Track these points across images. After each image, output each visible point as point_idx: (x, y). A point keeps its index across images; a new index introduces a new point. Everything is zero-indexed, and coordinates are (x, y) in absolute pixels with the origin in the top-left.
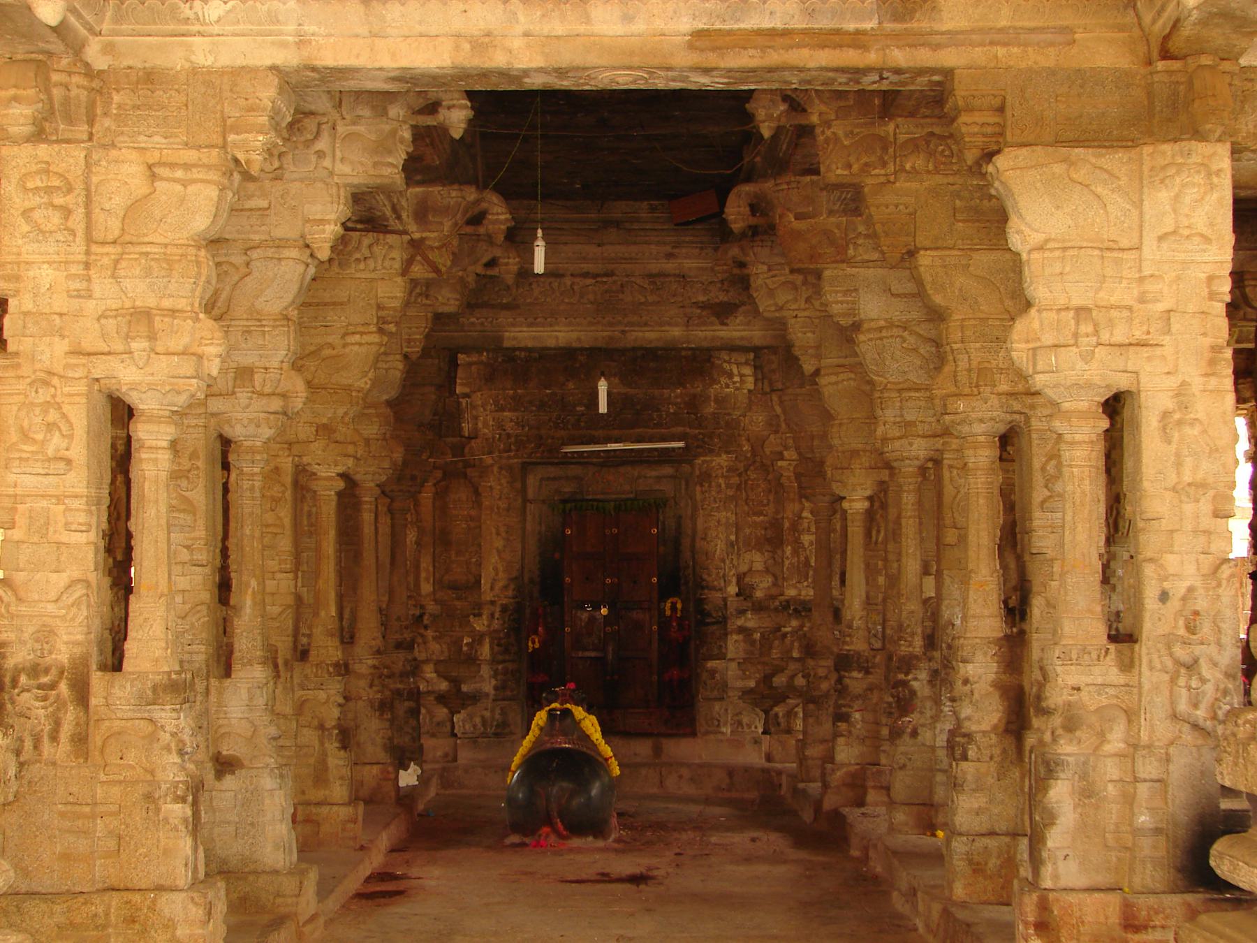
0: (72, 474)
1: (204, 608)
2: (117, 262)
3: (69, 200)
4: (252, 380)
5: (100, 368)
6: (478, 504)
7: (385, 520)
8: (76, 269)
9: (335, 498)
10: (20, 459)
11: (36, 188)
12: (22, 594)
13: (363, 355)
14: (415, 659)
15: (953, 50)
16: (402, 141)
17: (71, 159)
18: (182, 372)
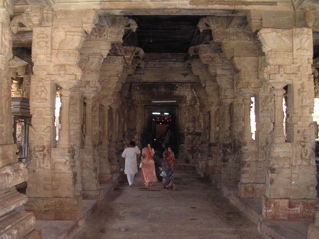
0: (47, 102)
1: (79, 134)
2: (57, 54)
3: (48, 40)
4: (89, 84)
5: (53, 78)
6: (136, 113)
7: (118, 117)
8: (49, 55)
9: (107, 111)
10: (36, 99)
11: (40, 37)
12: (36, 130)
13: (114, 84)
14: (123, 144)
15: (250, 6)
16: (122, 32)
17: (48, 31)
18: (72, 79)
